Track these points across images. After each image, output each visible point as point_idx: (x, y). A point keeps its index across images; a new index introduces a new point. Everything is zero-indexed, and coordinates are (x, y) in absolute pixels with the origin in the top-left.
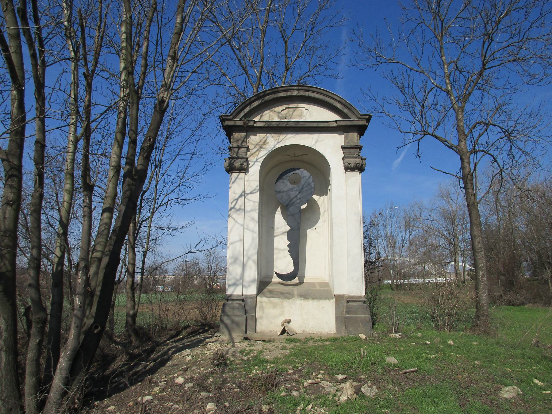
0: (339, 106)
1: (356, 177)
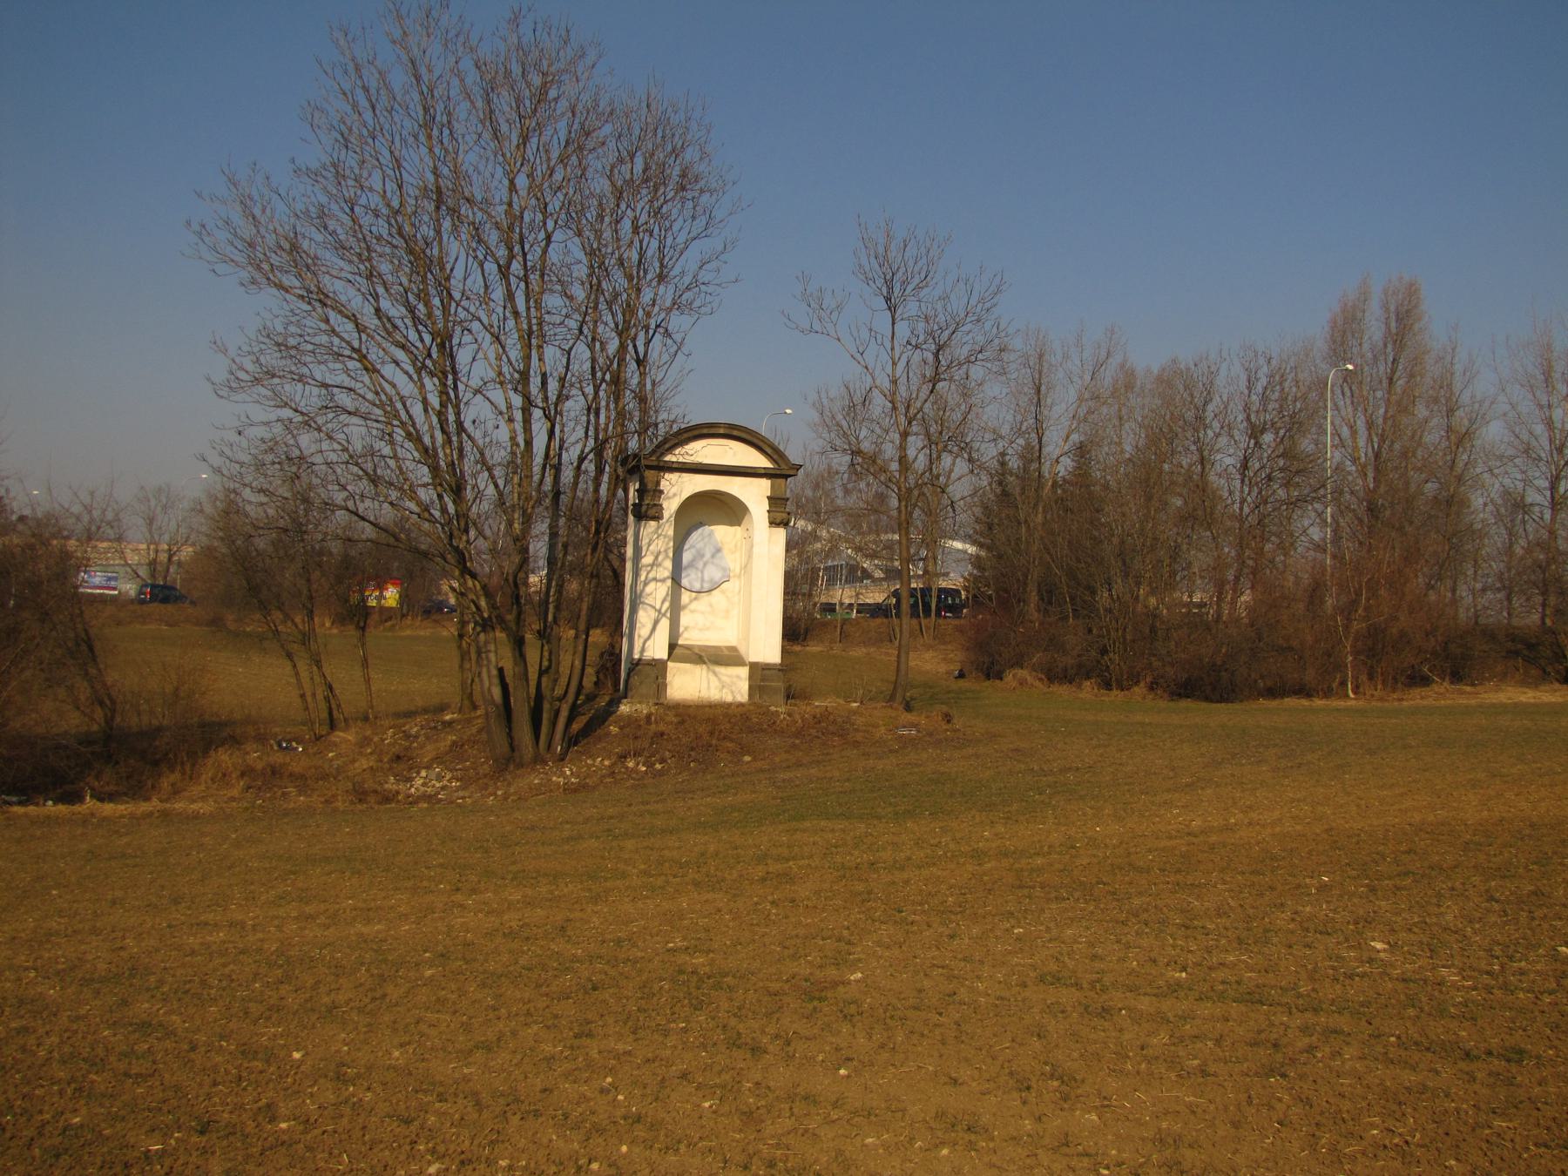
0: (769, 451)
1: (780, 535)
